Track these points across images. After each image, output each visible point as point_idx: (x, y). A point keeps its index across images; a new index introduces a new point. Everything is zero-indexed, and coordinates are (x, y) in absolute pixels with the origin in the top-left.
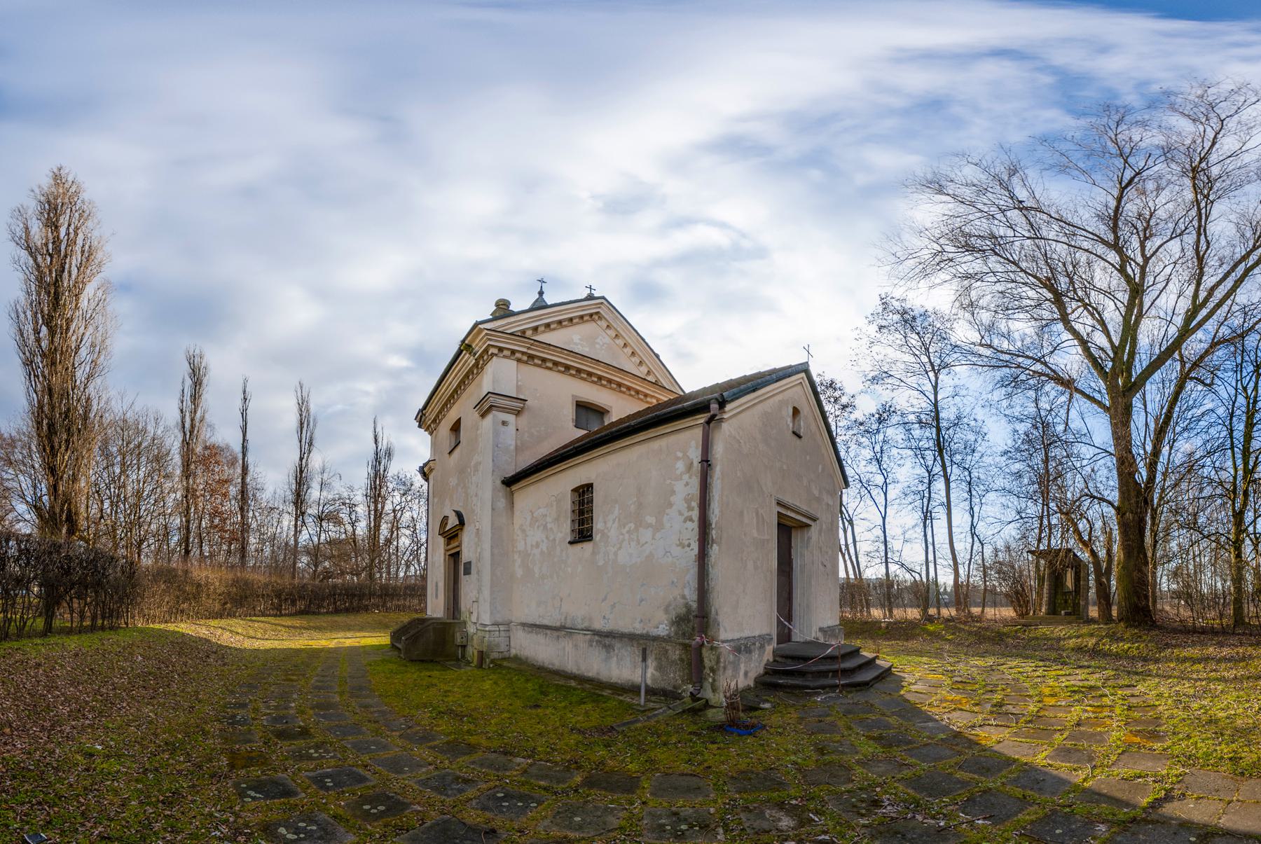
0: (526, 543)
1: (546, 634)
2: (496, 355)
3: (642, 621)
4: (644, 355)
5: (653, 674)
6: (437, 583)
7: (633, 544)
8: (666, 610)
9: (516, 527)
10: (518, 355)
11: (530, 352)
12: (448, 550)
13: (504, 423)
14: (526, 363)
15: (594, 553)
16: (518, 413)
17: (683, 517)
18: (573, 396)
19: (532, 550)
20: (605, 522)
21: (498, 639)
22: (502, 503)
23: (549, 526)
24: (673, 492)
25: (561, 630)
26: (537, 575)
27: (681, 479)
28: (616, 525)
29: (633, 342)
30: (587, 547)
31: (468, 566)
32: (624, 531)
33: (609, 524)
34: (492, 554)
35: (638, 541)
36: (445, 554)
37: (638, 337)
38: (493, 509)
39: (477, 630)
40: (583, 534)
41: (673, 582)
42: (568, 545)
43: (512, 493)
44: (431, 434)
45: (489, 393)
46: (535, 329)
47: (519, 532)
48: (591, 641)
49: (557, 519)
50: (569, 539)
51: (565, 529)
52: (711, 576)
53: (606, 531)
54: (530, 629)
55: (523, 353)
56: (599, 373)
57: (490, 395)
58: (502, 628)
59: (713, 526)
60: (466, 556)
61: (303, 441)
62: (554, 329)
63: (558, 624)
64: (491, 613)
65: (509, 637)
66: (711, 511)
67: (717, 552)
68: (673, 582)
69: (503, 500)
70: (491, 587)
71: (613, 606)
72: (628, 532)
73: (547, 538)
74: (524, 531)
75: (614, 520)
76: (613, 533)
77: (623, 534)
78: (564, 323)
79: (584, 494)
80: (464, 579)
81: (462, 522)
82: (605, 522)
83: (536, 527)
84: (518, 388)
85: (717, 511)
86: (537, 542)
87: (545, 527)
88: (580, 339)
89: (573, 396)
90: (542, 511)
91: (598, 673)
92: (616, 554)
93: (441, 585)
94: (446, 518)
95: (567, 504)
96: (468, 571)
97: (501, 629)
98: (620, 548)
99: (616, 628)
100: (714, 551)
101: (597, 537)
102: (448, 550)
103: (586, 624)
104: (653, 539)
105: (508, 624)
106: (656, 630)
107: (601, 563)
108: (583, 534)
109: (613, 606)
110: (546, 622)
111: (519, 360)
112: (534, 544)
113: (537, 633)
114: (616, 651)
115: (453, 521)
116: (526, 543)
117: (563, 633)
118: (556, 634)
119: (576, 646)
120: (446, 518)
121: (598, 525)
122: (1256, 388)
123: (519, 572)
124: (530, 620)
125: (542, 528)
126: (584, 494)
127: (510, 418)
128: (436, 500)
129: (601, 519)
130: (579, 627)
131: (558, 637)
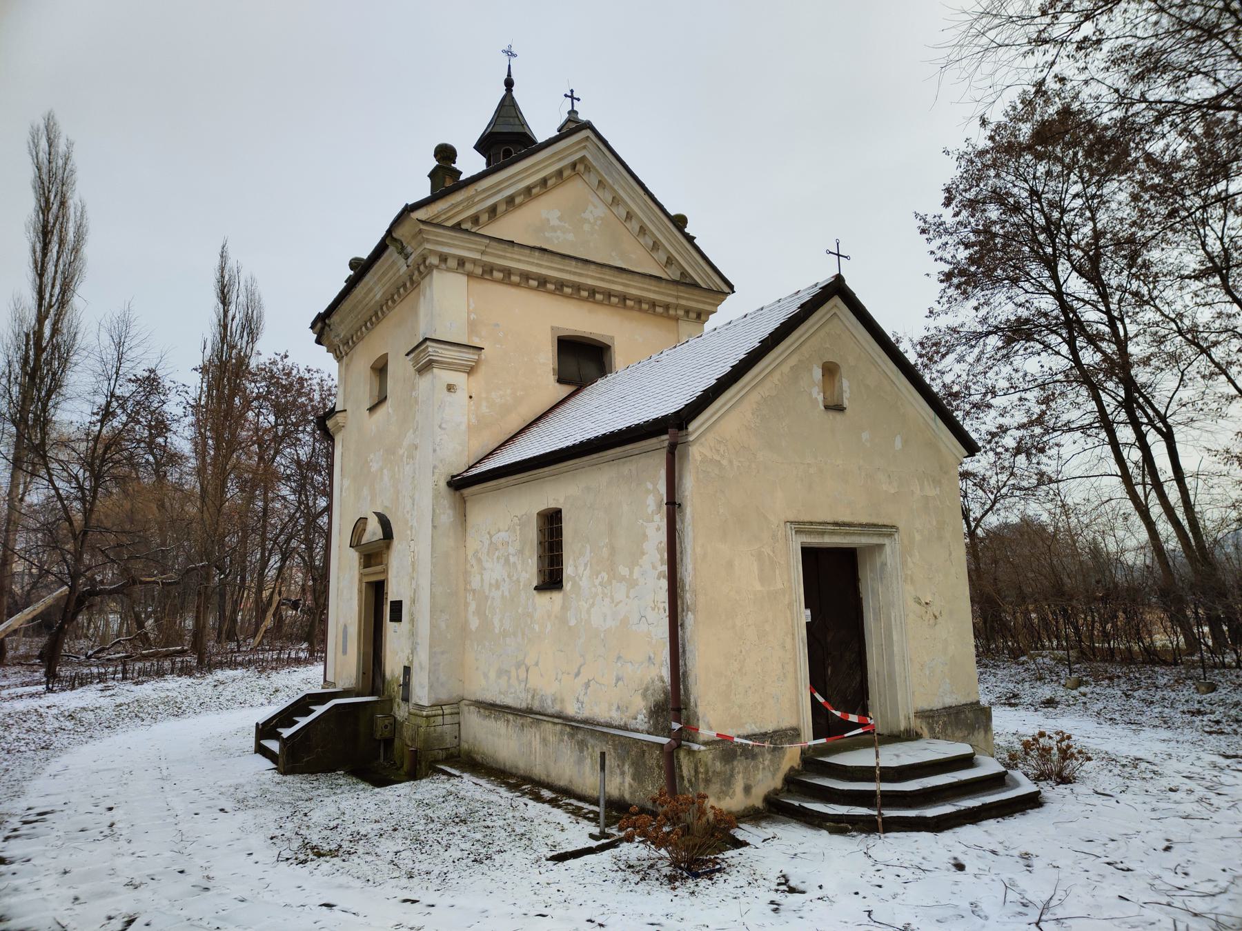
0: (482, 580)
1: (508, 721)
2: (437, 267)
3: (618, 707)
4: (659, 229)
5: (631, 786)
6: (345, 626)
7: (607, 600)
8: (644, 696)
9: (470, 553)
10: (468, 266)
11: (486, 259)
12: (366, 575)
13: (450, 388)
14: (481, 277)
15: (565, 608)
16: (471, 370)
17: (657, 572)
18: (552, 328)
19: (490, 590)
20: (576, 567)
21: (443, 727)
22: (447, 516)
23: (512, 559)
24: (645, 536)
25: (527, 715)
26: (497, 631)
27: (653, 521)
28: (587, 572)
29: (640, 207)
30: (556, 596)
31: (397, 607)
32: (597, 582)
33: (581, 569)
34: (433, 596)
35: (612, 597)
36: (360, 581)
37: (646, 198)
38: (434, 527)
39: (410, 713)
40: (551, 579)
41: (650, 658)
42: (535, 592)
43: (464, 501)
44: (339, 358)
45: (426, 339)
46: (475, 220)
47: (474, 562)
48: (562, 733)
49: (521, 552)
50: (535, 584)
51: (530, 571)
52: (508, 764)
53: (577, 578)
54: (487, 713)
55: (474, 262)
56: (590, 282)
57: (428, 343)
58: (447, 710)
59: (687, 588)
60: (392, 594)
61: (51, 269)
62: (521, 205)
63: (524, 705)
64: (431, 687)
65: (459, 723)
66: (684, 568)
67: (692, 622)
68: (650, 658)
69: (450, 512)
70: (431, 647)
71: (587, 685)
72: (601, 584)
73: (509, 576)
74: (479, 561)
75: (586, 565)
76: (584, 583)
77: (595, 586)
78: (535, 191)
79: (551, 522)
80: (390, 627)
81: (388, 533)
82: (576, 567)
83: (495, 557)
84: (472, 326)
85: (690, 567)
86: (497, 581)
87: (507, 560)
88: (560, 219)
89: (552, 328)
90: (503, 535)
91: (571, 781)
92: (588, 611)
93: (353, 631)
94: (363, 520)
95: (532, 534)
96: (397, 615)
97: (446, 712)
98: (593, 605)
99: (591, 716)
100: (689, 619)
101: (567, 585)
102: (366, 575)
103: (557, 708)
104: (627, 597)
105: (458, 703)
106: (634, 721)
107: (573, 622)
108: (551, 579)
109: (587, 685)
110: (509, 701)
111: (470, 275)
112: (493, 582)
113: (496, 719)
114: (590, 750)
115: (373, 530)
116: (482, 580)
117: (529, 720)
118: (520, 721)
119: (544, 741)
120: (363, 520)
121: (568, 570)
122: (201, 927)
123: (474, 623)
124: (489, 697)
125: (502, 561)
126: (551, 522)
127: (459, 379)
128: (346, 483)
129: (571, 562)
130: (550, 711)
131: (522, 725)
